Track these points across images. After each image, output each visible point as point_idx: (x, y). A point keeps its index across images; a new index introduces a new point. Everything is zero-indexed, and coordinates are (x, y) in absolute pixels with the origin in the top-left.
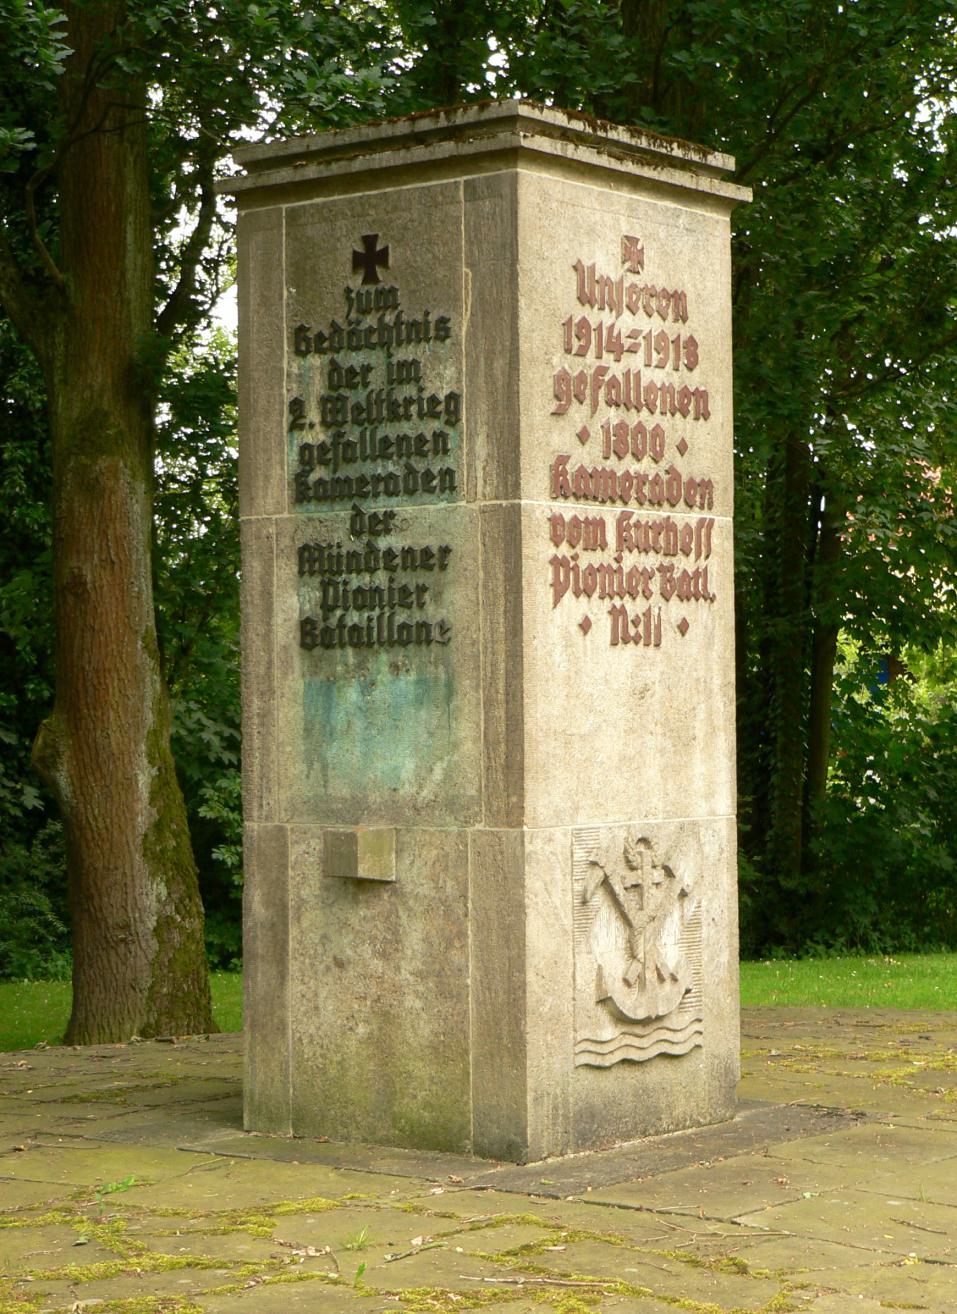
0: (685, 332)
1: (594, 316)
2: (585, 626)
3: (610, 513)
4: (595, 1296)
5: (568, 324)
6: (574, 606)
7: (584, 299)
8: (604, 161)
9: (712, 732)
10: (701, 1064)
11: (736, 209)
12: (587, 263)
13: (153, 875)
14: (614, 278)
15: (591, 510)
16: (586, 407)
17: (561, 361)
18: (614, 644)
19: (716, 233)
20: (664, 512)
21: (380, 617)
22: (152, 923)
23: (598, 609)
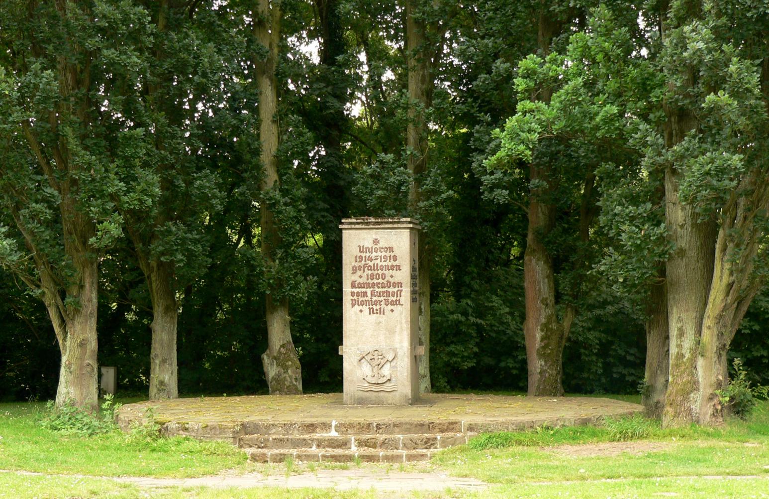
0: (392, 254)
1: (363, 255)
2: (392, 311)
3: (369, 291)
4: (431, 442)
5: (356, 257)
6: (357, 308)
7: (360, 252)
8: (363, 226)
9: (401, 330)
10: (397, 394)
11: (411, 228)
12: (362, 245)
13: (540, 359)
14: (370, 247)
15: (364, 290)
16: (362, 271)
17: (354, 264)
18: (370, 314)
19: (406, 234)
20: (387, 289)
21: (380, 308)
22: (539, 370)
23: (366, 309)
